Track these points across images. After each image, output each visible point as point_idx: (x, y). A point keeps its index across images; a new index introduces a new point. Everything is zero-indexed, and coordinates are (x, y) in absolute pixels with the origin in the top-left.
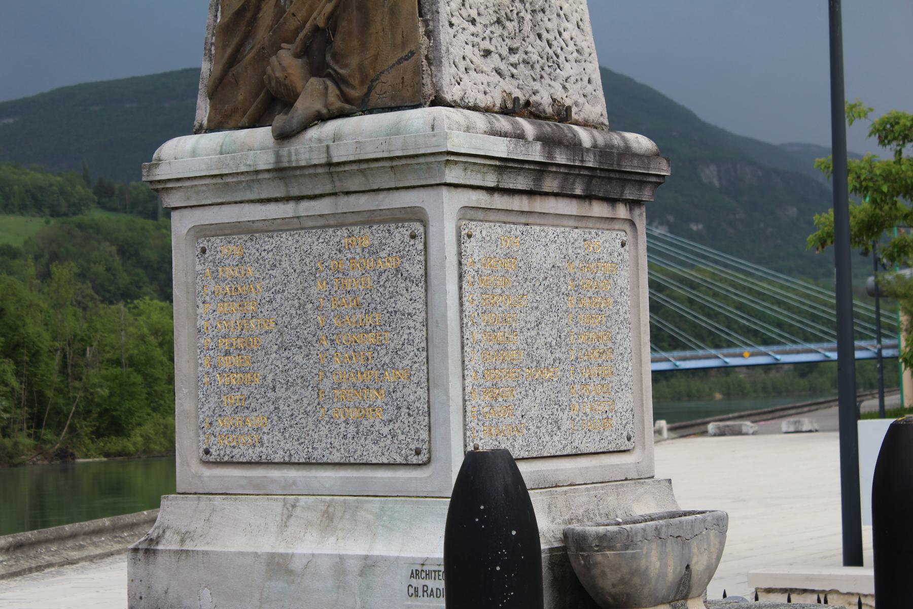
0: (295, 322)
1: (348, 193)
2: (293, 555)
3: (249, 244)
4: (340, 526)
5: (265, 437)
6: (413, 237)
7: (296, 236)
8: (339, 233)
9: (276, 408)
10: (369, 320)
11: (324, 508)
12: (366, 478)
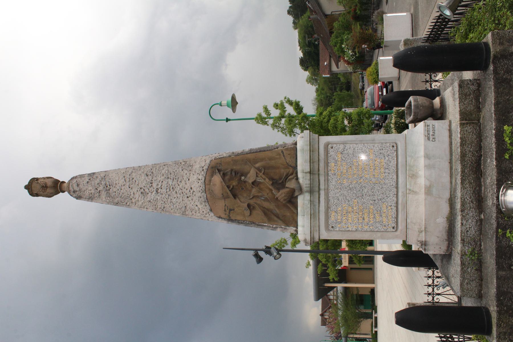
0: (355, 192)
1: (319, 170)
2: (425, 185)
3: (331, 209)
5: (389, 204)
6: (332, 148)
11: (410, 178)
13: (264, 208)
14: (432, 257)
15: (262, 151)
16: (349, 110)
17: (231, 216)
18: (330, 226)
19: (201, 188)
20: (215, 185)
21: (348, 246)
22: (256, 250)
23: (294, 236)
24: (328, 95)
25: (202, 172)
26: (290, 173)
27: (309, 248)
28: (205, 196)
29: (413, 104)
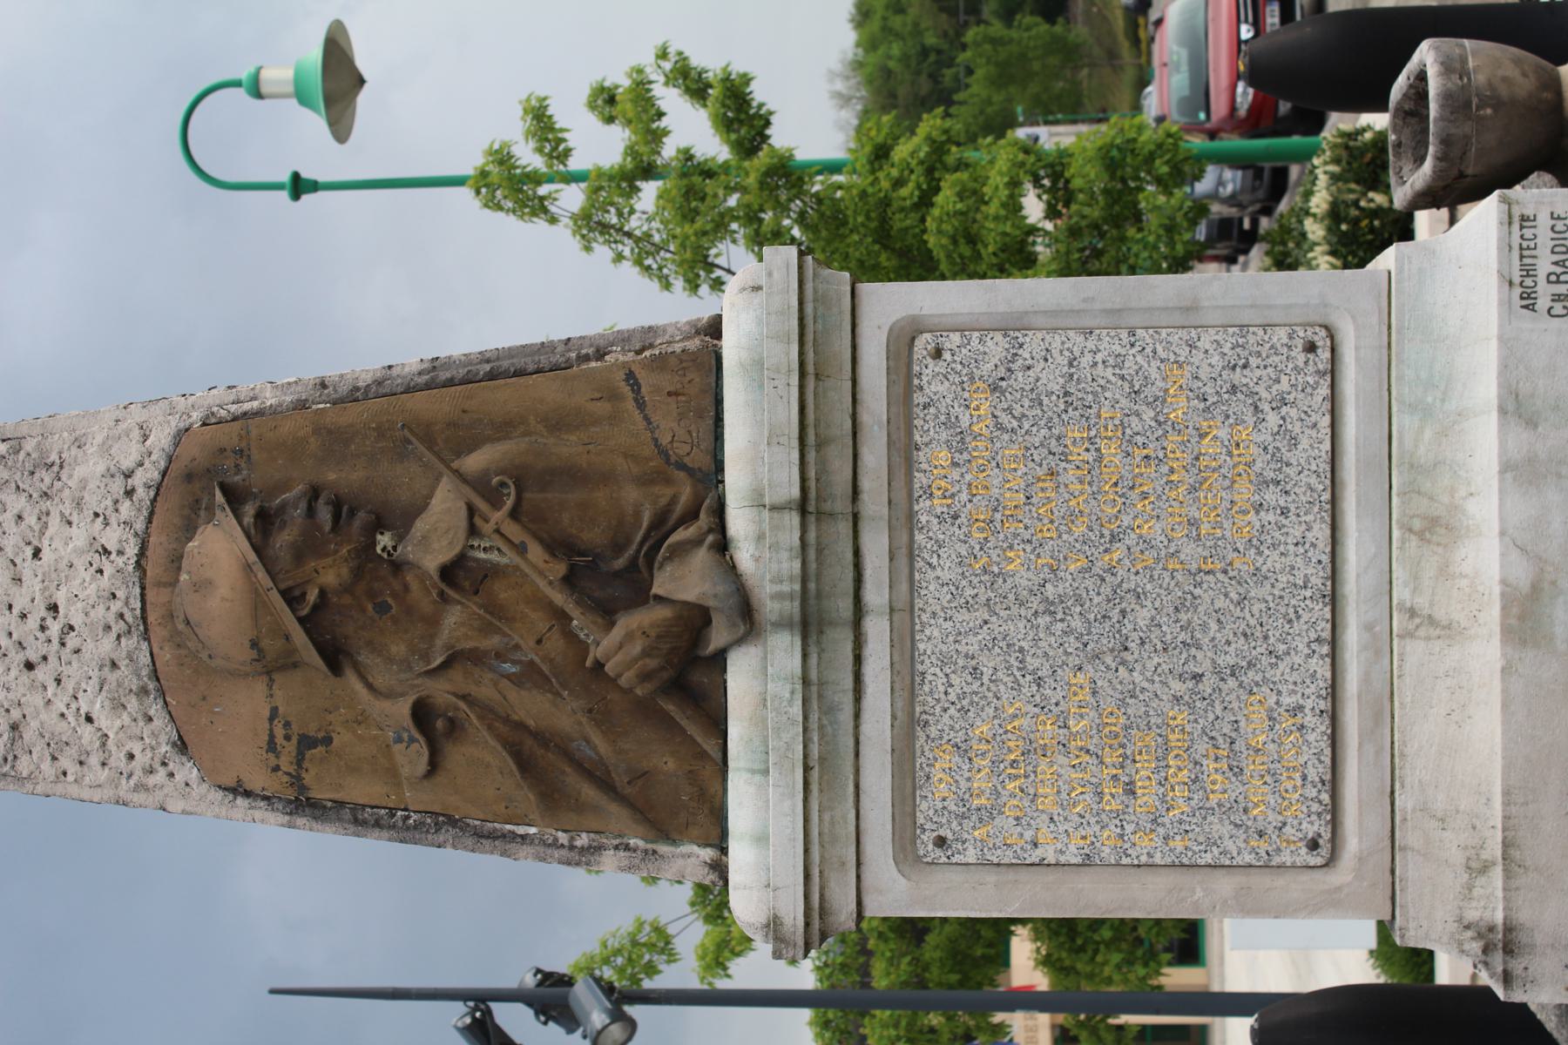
0: (1077, 623)
2: (1504, 582)
3: (933, 731)
4: (1446, 499)
5: (1287, 700)
6: (938, 354)
7: (924, 617)
8: (923, 519)
9: (1233, 675)
10: (1079, 454)
11: (1414, 541)
12: (1358, 460)
13: (521, 726)
14: (1551, 1023)
15: (506, 374)
16: (1054, 137)
17: (308, 778)
18: (929, 837)
19: (116, 606)
20: (202, 586)
21: (1047, 962)
22: (481, 1000)
23: (713, 899)
24: (931, 40)
25: (126, 507)
26: (679, 509)
27: (804, 976)
28: (144, 659)
29: (1434, 87)
